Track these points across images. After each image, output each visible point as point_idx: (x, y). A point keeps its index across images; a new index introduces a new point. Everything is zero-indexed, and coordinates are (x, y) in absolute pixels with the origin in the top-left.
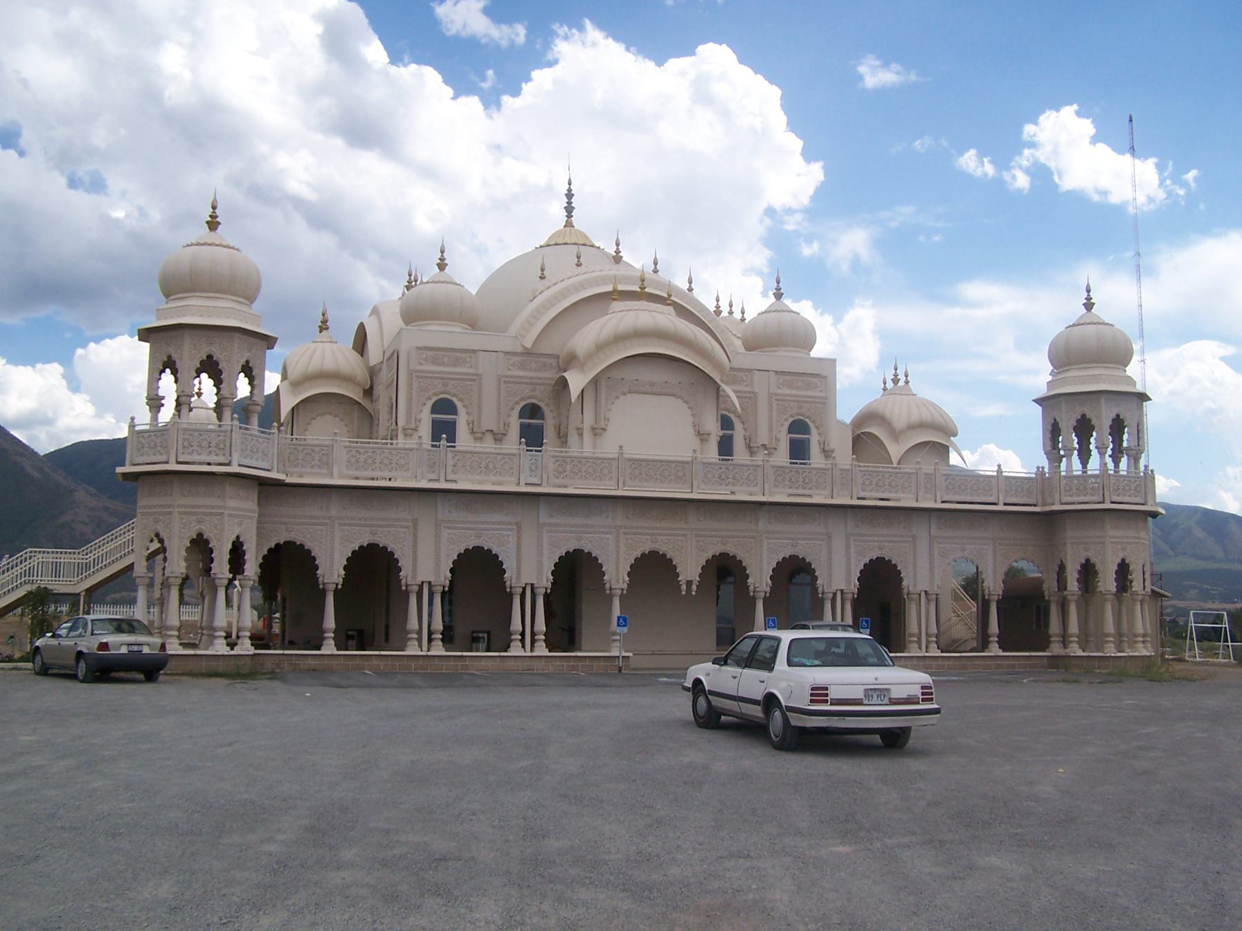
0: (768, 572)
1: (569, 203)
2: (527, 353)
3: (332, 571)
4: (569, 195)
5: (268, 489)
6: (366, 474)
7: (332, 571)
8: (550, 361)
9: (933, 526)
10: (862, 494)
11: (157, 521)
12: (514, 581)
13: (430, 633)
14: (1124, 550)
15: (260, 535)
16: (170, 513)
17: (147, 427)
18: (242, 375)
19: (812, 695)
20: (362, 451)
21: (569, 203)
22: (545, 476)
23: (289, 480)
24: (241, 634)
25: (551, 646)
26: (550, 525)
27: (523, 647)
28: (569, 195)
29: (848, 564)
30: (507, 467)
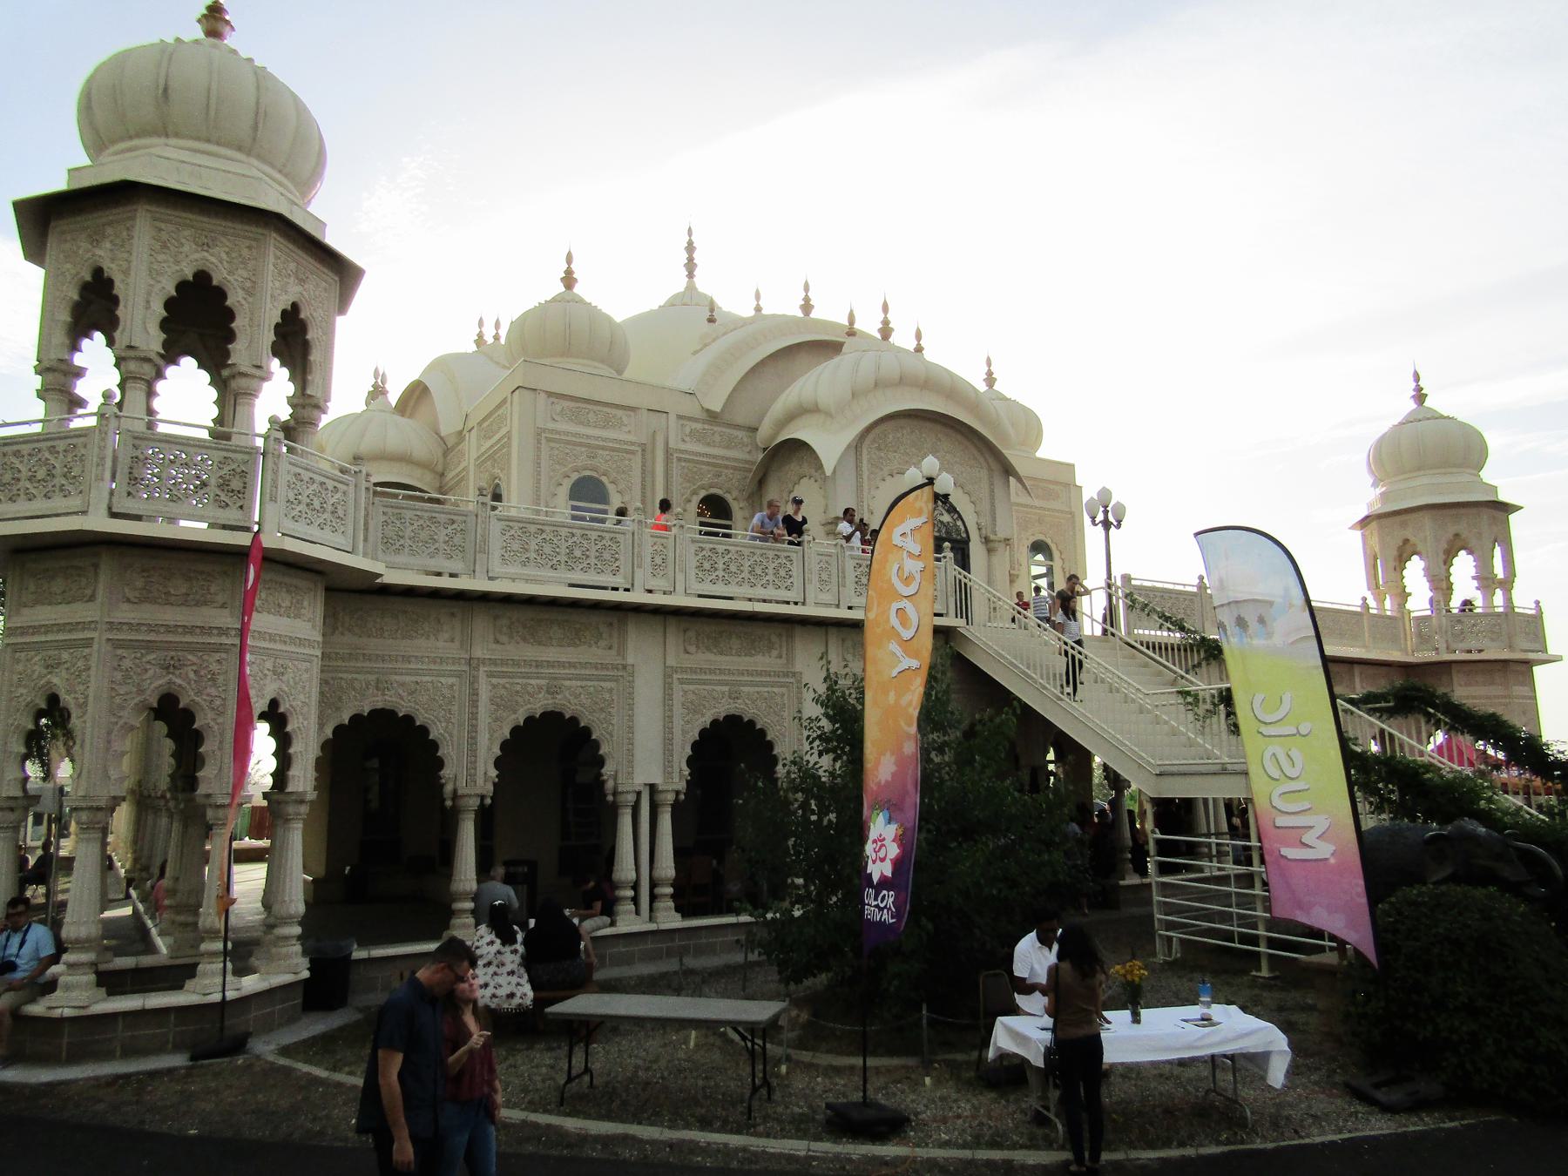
0: (488, 749)
1: (691, 259)
2: (712, 417)
3: (471, 767)
4: (690, 248)
5: (349, 595)
6: (751, 592)
7: (471, 767)
8: (740, 434)
9: (671, 640)
10: (651, 585)
11: (50, 667)
12: (461, 783)
13: (653, 884)
14: (278, 673)
15: (328, 700)
16: (88, 643)
17: (37, 428)
18: (276, 363)
19: (1205, 801)
20: (408, 514)
21: (691, 259)
22: (680, 577)
23: (392, 577)
24: (659, 890)
25: (684, 910)
26: (493, 662)
27: (637, 913)
28: (690, 248)
29: (668, 719)
30: (424, 535)
